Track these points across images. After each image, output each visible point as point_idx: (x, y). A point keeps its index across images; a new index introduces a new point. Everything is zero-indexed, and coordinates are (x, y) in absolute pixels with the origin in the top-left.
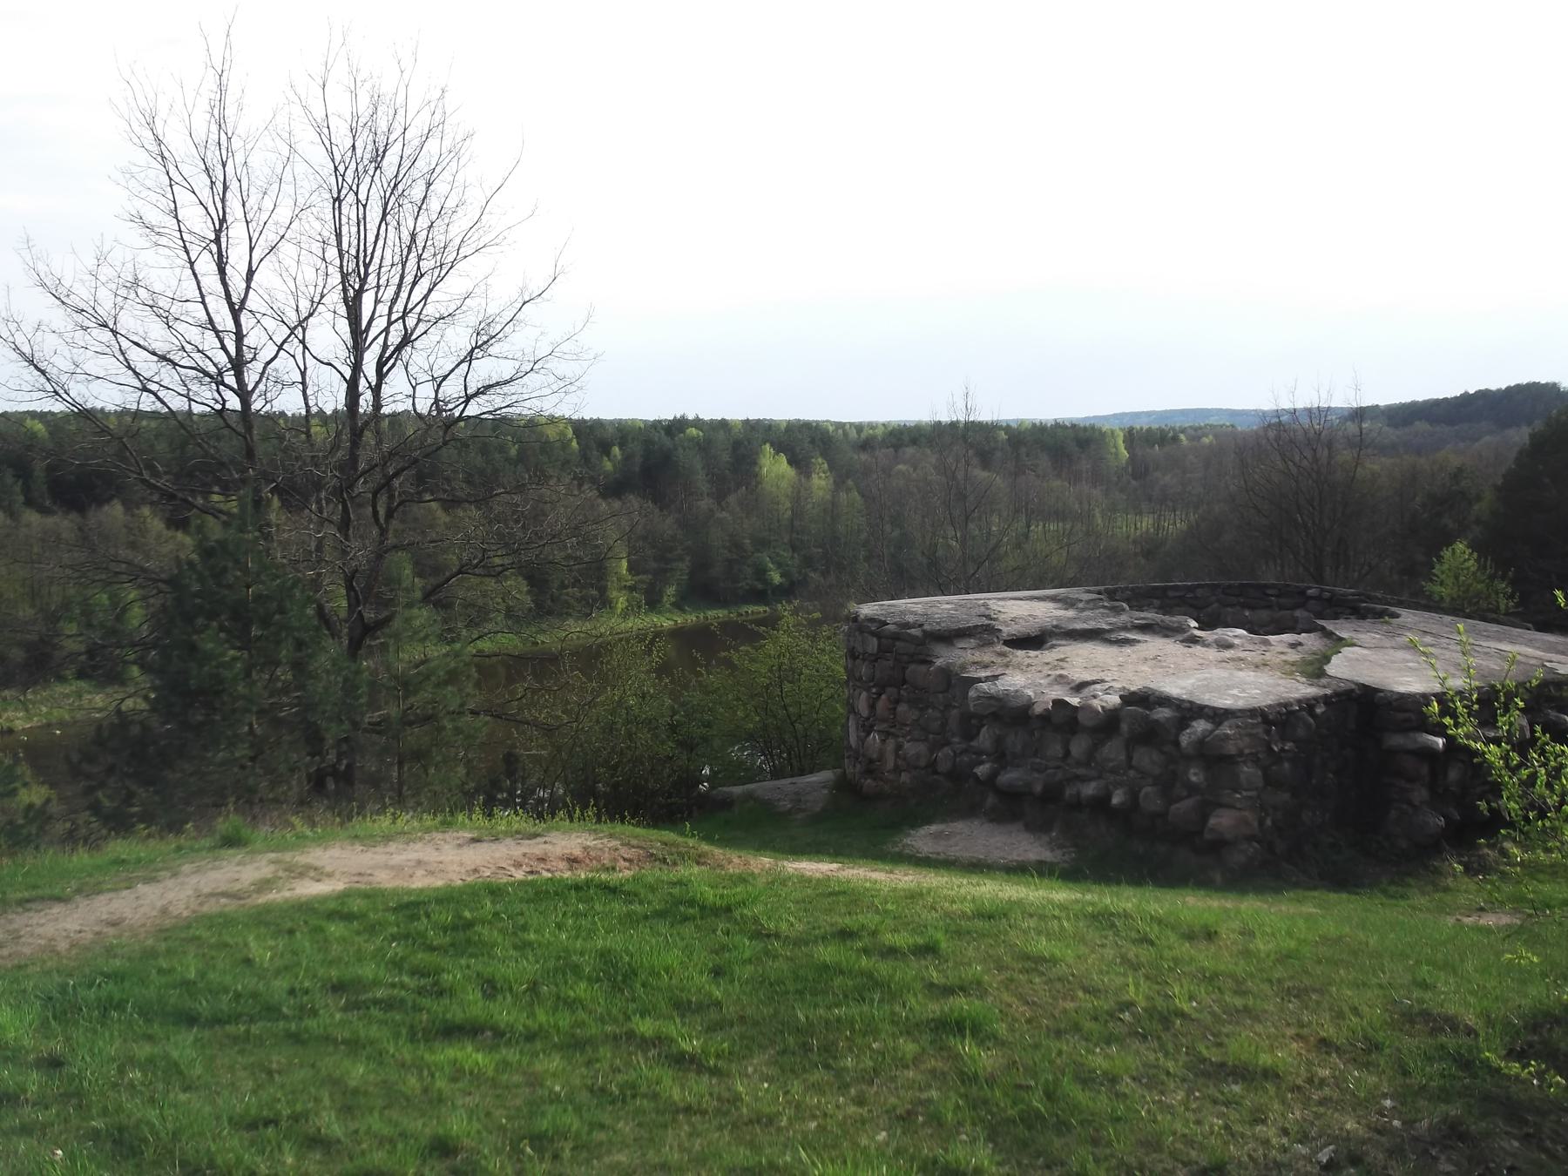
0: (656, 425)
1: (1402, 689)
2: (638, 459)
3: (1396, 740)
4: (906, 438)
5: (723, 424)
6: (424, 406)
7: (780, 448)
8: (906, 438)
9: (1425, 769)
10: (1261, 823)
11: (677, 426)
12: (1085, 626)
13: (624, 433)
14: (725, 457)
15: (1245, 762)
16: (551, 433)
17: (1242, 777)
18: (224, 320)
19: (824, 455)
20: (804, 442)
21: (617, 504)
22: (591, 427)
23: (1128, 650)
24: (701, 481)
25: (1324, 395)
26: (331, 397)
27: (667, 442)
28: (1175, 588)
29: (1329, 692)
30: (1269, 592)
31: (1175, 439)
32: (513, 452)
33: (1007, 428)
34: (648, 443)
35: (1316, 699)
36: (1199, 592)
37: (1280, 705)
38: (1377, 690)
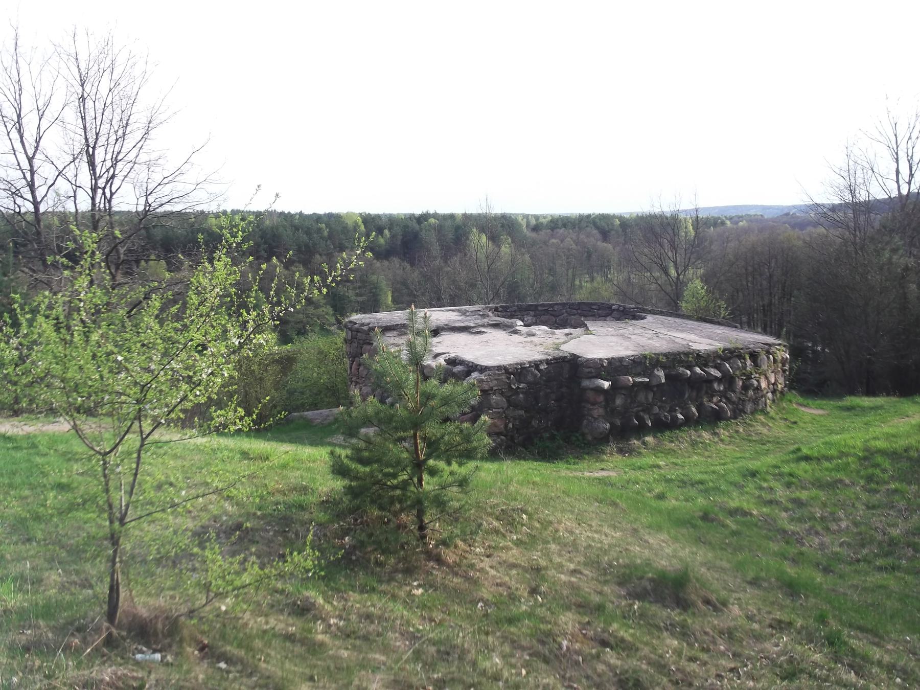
0: (412, 217)
1: (589, 356)
2: (400, 237)
3: (586, 383)
4: (560, 223)
5: (452, 216)
6: (141, 208)
7: (482, 230)
8: (560, 223)
9: (601, 398)
10: (506, 426)
11: (422, 219)
12: (462, 325)
13: (392, 222)
14: (450, 236)
15: (494, 394)
16: (350, 223)
17: (492, 402)
18: (25, 165)
19: (510, 234)
20: (500, 227)
21: (386, 263)
22: (373, 218)
23: (477, 337)
24: (436, 249)
25: (657, 205)
26: (84, 204)
27: (417, 227)
28: (543, 305)
29: (550, 358)
30: (594, 307)
31: (723, 223)
32: (326, 233)
33: (620, 218)
34: (406, 227)
35: (541, 362)
36: (556, 308)
37: (517, 364)
38: (579, 357)
